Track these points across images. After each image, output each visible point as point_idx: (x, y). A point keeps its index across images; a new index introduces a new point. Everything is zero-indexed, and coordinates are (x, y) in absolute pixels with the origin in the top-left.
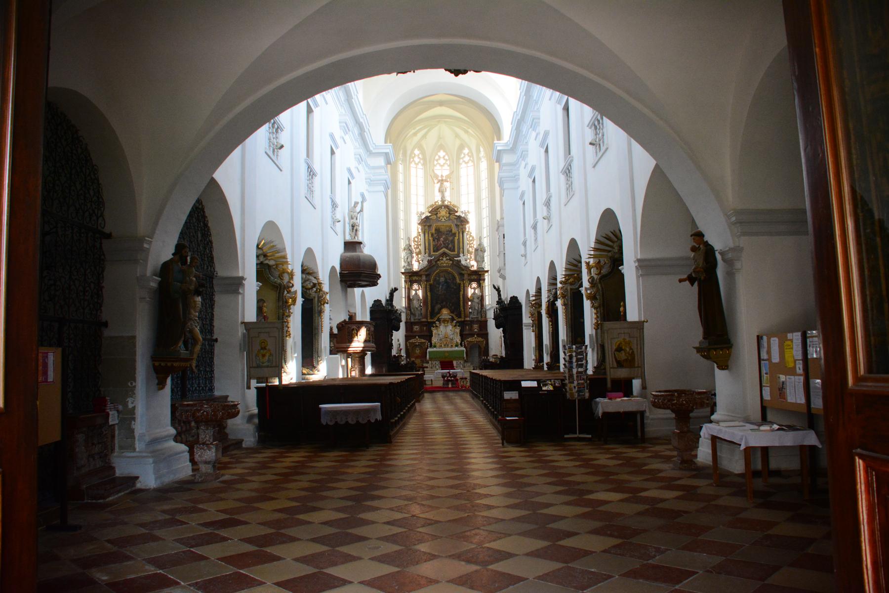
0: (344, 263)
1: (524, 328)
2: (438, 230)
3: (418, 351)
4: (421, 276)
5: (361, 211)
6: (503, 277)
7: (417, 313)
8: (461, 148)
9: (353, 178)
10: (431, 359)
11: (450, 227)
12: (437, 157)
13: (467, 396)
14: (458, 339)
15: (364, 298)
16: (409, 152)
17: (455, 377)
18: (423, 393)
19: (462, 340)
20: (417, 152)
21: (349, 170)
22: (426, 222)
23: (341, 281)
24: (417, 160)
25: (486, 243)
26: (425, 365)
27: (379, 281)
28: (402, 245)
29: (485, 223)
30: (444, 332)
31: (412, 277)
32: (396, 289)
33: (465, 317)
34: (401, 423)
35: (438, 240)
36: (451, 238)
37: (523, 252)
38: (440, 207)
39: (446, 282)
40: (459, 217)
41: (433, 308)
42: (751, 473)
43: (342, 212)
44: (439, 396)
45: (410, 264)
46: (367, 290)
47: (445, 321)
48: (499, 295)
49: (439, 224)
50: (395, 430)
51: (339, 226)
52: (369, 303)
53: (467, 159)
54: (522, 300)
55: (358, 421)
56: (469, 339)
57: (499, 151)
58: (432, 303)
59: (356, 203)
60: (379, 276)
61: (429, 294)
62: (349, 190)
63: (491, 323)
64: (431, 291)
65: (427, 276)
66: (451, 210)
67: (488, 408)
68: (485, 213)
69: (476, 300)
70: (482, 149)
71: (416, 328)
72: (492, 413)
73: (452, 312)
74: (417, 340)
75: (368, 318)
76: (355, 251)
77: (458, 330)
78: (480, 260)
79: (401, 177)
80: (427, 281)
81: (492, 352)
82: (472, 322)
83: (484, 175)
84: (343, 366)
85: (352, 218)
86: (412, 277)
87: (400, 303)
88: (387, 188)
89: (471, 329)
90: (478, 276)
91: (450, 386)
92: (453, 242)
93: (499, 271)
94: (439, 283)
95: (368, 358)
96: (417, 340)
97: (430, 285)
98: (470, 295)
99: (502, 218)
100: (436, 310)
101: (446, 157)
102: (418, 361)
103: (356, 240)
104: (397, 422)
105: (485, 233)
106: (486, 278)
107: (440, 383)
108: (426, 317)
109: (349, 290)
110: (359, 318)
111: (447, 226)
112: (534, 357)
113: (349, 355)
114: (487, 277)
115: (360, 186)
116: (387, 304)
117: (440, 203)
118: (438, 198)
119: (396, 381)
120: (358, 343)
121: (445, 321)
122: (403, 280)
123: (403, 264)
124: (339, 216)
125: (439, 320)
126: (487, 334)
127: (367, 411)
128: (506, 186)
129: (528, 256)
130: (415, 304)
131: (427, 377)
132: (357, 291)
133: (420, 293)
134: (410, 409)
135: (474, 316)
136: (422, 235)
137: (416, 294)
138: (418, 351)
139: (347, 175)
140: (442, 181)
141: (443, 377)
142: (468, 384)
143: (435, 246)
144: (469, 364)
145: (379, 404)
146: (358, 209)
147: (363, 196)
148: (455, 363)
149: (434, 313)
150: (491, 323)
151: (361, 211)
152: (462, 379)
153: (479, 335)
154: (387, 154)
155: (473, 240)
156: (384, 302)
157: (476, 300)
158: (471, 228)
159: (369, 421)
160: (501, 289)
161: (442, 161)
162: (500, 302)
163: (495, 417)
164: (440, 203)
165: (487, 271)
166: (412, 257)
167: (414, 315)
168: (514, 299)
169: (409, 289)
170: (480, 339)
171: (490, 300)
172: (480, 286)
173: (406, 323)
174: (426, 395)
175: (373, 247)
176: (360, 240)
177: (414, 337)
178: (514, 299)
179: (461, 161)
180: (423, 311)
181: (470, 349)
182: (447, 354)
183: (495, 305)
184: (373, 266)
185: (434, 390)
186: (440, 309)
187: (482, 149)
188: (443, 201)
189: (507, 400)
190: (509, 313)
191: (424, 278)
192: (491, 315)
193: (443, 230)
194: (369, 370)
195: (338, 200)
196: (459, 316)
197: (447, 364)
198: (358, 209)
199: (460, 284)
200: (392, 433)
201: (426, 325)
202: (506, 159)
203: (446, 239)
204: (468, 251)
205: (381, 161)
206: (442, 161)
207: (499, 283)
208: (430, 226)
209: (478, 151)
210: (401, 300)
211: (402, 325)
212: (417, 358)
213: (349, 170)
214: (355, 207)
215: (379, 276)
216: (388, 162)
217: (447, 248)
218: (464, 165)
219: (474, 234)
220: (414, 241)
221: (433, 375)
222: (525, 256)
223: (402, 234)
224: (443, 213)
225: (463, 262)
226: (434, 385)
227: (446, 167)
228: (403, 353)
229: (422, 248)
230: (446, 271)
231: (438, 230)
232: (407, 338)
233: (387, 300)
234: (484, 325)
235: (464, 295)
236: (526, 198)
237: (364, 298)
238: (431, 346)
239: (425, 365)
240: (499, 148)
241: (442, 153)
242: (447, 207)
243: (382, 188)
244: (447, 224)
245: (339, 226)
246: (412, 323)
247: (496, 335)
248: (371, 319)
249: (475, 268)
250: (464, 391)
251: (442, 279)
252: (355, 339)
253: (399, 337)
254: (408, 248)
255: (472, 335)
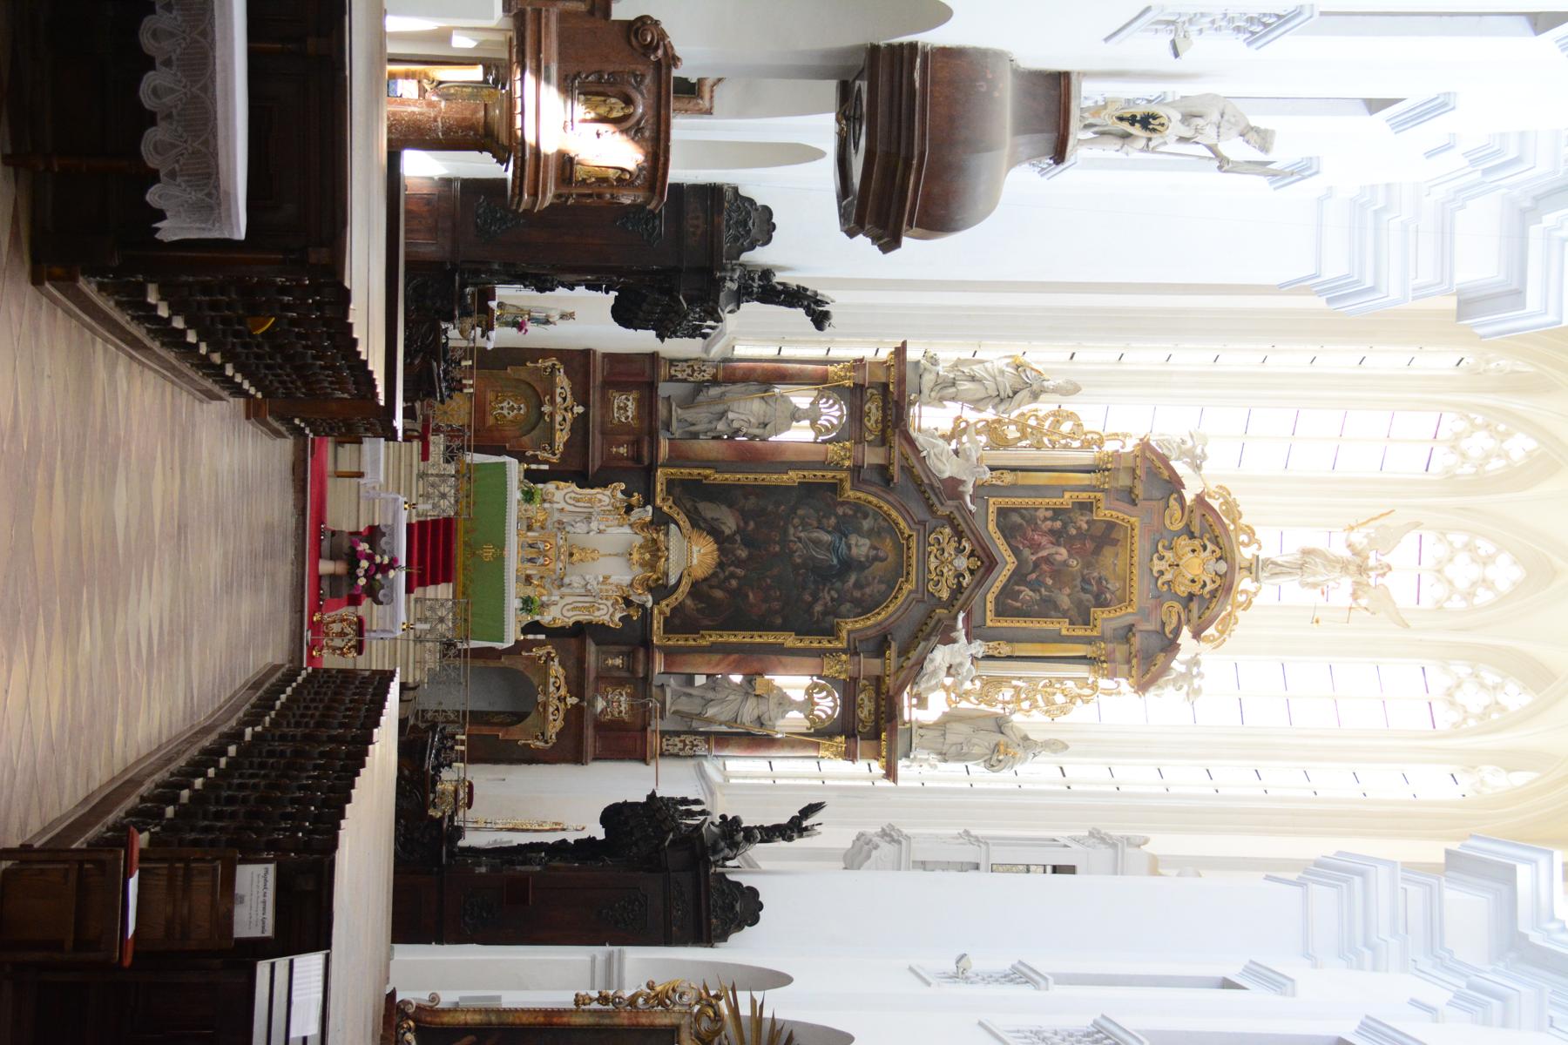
0: (956, 64)
1: (600, 952)
2: (1107, 536)
3: (509, 409)
4: (883, 441)
5: (1223, 164)
6: (857, 856)
7: (699, 416)
8: (1536, 675)
9: (1399, 125)
10: (467, 475)
11: (1124, 599)
12: (1485, 547)
13: (273, 652)
14: (559, 613)
15: (781, 160)
16: (1518, 404)
17: (372, 591)
18: (298, 432)
19: (555, 634)
20: (1520, 446)
21: (1438, 106)
22: (1151, 477)
23: (874, 50)
24: (1479, 443)
25: (1035, 772)
26: (438, 444)
27: (863, 241)
28: (1045, 357)
29: (1137, 777)
30: (594, 540)
31: (881, 397)
32: (820, 320)
33: (670, 653)
34: (139, 331)
35: (1058, 536)
36: (1064, 601)
37: (977, 965)
38: (1225, 555)
39: (848, 565)
40: (1171, 647)
41: (720, 494)
42: (490, 429)
43: (1222, 68)
44: (278, 507)
45: (946, 389)
46: (825, 173)
47: (655, 551)
48: (771, 833)
49: (1140, 544)
50: (107, 305)
51: (1150, 48)
52: (757, 184)
53: (1473, 698)
54: (741, 950)
55: (150, 119)
56: (556, 669)
57: (1508, 875)
58: (747, 490)
59: (1262, 138)
60: (888, 241)
61: (793, 477)
62: (1331, 104)
63: (628, 783)
64: (808, 489)
65: (883, 471)
66: (1205, 605)
67: (197, 767)
68: (1186, 779)
69: (749, 711)
70: (1520, 779)
71: (625, 407)
72: (167, 794)
73: (696, 589)
74: (563, 410)
75: (680, 172)
76: (1024, 126)
77: (607, 614)
78: (950, 740)
79: (1387, 359)
80: (856, 470)
81: (484, 778)
82: (642, 685)
83: (1384, 785)
84: (444, 36)
85: (1188, 117)
86: (881, 397)
87: (750, 334)
88: (1337, 293)
89: (607, 679)
90: (869, 724)
91: (326, 567)
92: (1048, 608)
93: (890, 835)
94: (843, 529)
95: (480, 165)
96: (563, 410)
97: (835, 487)
98: (780, 680)
99: (1154, 866)
100: (709, 511)
101: (1484, 596)
102: (458, 410)
103: (1077, 133)
104: (146, 314)
105: (1087, 773)
106: (861, 766)
107: (343, 514)
108: (677, 459)
109: (830, 88)
110: (684, 129)
111: (1127, 581)
112: (447, 998)
113: (498, 72)
114: (863, 771)
115: (1355, 154)
116: (748, 272)
117: (1247, 553)
118: (1268, 533)
119: (356, 316)
120: (564, 127)
121: (655, 551)
122: (867, 353)
123: (948, 354)
124: (1204, 49)
125: (661, 521)
126: (577, 758)
127: (204, 172)
128: (1323, 896)
129: (961, 989)
130: (746, 410)
131: (375, 451)
132: (822, 129)
133: (799, 434)
134: (216, 372)
135: (672, 696)
136: (1087, 457)
137: (796, 415)
138: (509, 409)
139: (1415, 93)
140: (1358, 566)
141: (373, 534)
142: (330, 661)
143: (1029, 516)
144: (432, 660)
145: (241, 233)
146: (1235, 149)
147: (1301, 171)
148: (443, 591)
149: (695, 496)
150: (628, 783)
151: (1223, 164)
152: (360, 626)
153: (575, 716)
154: (1514, 296)
155: (1052, 710)
156: (759, 256)
157: (749, 711)
158: (1114, 705)
159: (153, 177)
160: (799, 843)
161: (1463, 571)
162: (734, 834)
163: (145, 815)
164: (1247, 553)
165: (891, 773)
166: (977, 404)
167: (689, 402)
168: (743, 908)
169: (819, 380)
170: (555, 725)
171: (740, 784)
172: (819, 735)
173: (653, 357)
174: (286, 445)
175: (1027, 216)
176: (1075, 153)
177: (582, 396)
178: (743, 908)
179: (1462, 670)
180: (706, 447)
181: (507, 671)
182: (488, 553)
183: (722, 807)
184: (938, 217)
185: (306, 483)
186: (715, 532)
187: (1520, 779)
188: (1253, 568)
189: (230, 880)
190: (673, 876)
191: (873, 457)
192: (671, 780)
193: (1107, 564)
194: (423, 168)
195: (1284, 46)
196: (678, 623)
197: (435, 550)
198: (1235, 149)
199: (832, 632)
200: (88, 287)
201: (637, 458)
202: (1466, 907)
203: (1059, 572)
204: (998, 682)
205: (1478, 265)
206: (1463, 571)
207: (830, 834)
208: (1130, 496)
209: (1510, 761)
210: (765, 338)
211: (643, 340)
212: (480, 409)
213: (1438, 106)
214: (1248, 132)
215: (888, 241)
216: (1469, 304)
217: (1018, 576)
218: (1439, 680)
219: (1081, 714)
220: (1058, 416)
221: (384, 485)
222: (960, 973)
223: (1095, 355)
224: (1196, 566)
225: (941, 656)
226: (332, 485)
227: (1433, 592)
228: (502, 337)
229: (1024, 455)
230: (899, 570)
231: (1107, 536)
232: (578, 361)
233: (767, 273)
234: (625, 742)
235: (780, 650)
236: (1256, 994)
237: (781, 160)
238: (531, 476)
239: (438, 444)
240: (1524, 874)
241: (1505, 573)
242: (1225, 587)
243: (1335, 268)
244: (1140, 590)
245: (1150, 48)
246: (652, 387)
247: (564, 802)
248: (677, 188)
249: (910, 712)
250: (297, 636)
251: (860, 547)
252: (581, 111)
253: (584, 318)
254: (1023, 385)
255: (577, 684)
